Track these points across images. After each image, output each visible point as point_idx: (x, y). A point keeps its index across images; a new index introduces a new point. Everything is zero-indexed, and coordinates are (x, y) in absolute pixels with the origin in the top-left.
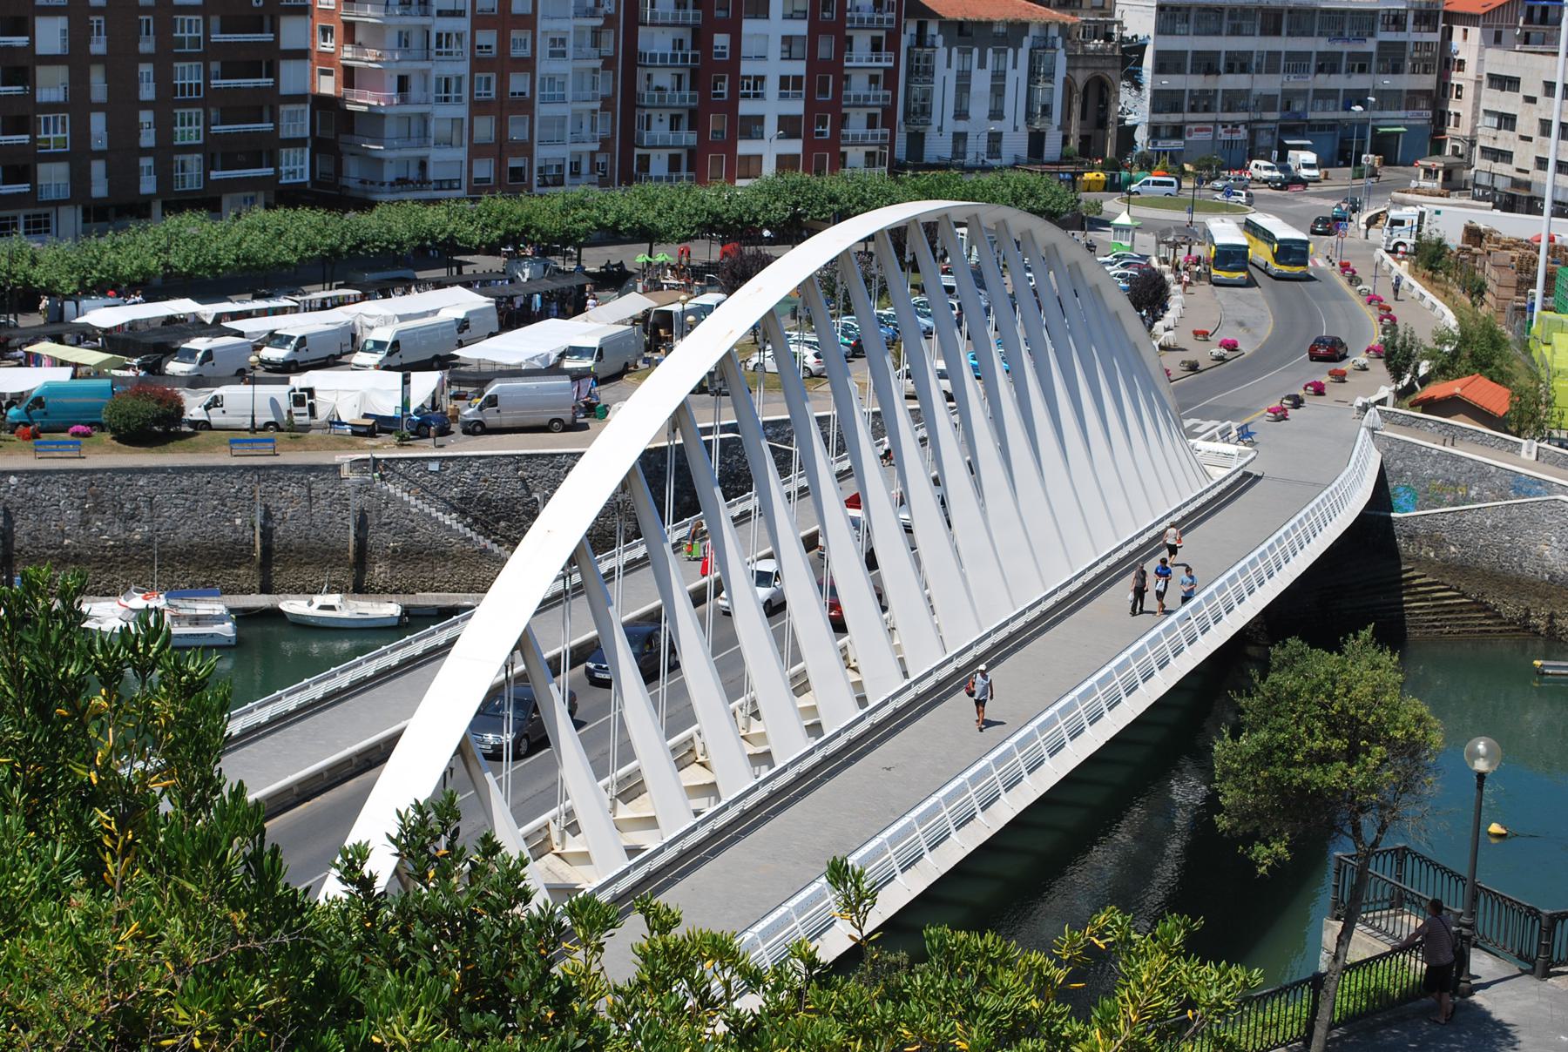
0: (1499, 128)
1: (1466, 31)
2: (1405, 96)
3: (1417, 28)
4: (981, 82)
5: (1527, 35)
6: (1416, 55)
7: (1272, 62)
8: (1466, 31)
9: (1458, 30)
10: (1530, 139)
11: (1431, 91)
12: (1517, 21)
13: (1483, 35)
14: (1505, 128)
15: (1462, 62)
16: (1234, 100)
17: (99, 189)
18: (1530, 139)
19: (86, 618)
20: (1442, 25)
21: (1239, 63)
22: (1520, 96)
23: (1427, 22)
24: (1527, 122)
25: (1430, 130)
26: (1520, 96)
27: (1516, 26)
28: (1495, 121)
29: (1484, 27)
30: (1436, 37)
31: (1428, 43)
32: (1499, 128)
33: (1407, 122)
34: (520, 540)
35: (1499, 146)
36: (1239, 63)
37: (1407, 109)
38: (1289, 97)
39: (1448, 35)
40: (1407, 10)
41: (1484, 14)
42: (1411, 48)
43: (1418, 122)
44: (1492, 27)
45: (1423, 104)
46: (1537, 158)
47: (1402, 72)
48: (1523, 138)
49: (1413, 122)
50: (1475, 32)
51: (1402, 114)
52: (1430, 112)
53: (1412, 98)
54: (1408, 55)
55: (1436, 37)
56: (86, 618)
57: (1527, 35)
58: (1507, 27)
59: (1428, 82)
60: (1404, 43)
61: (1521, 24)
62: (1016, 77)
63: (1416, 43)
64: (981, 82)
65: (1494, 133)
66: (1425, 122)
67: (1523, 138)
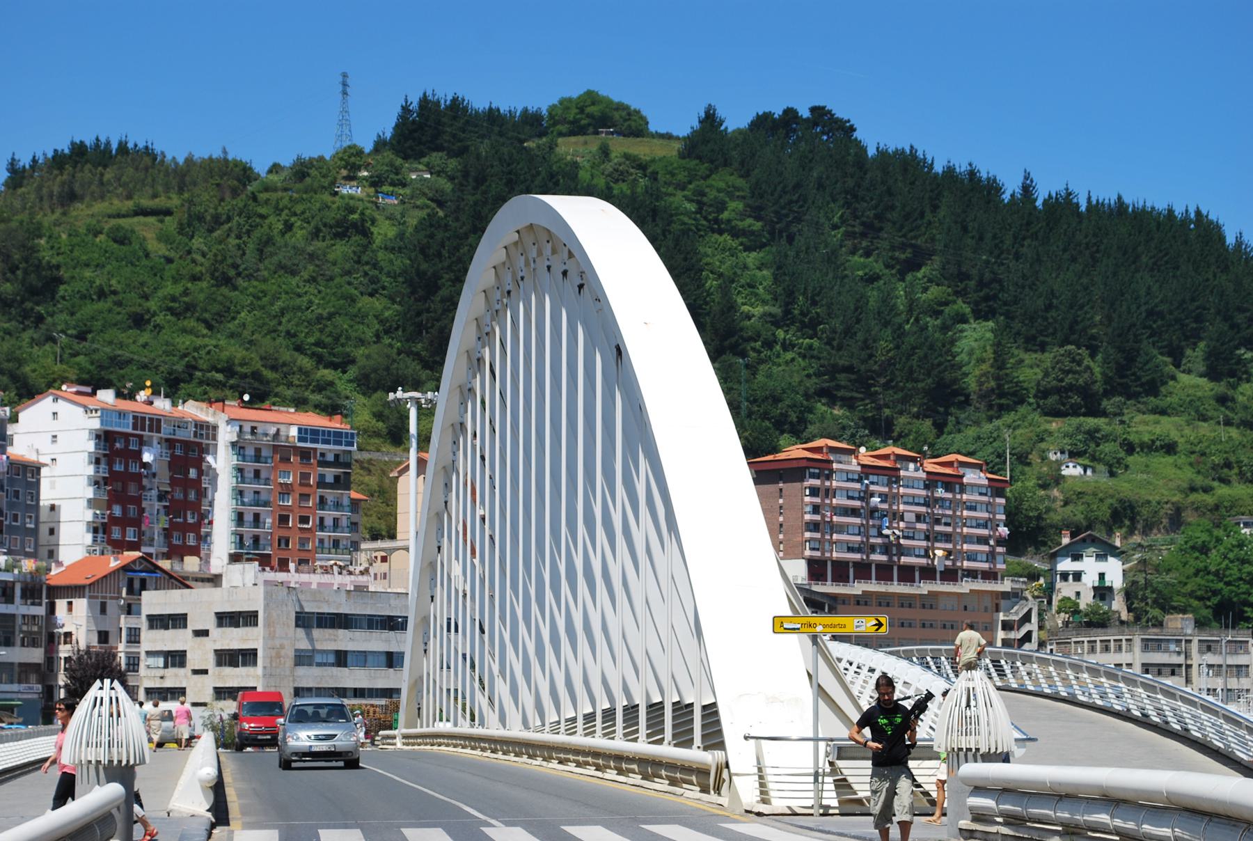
0: (166, 666)
1: (70, 603)
2: (17, 669)
3: (24, 601)
5: (129, 606)
6: (25, 628)
8: (70, 603)
9: (61, 605)
10: (205, 672)
11: (39, 665)
12: (120, 592)
13: (90, 606)
14: (174, 665)
15: (68, 635)
18: (205, 672)
19: (24, 167)
20: (45, 601)
22: (189, 631)
23: (32, 597)
24: (200, 654)
25: (40, 706)
26: (189, 631)
27: (119, 597)
28: (160, 661)
29: (90, 597)
30: (40, 611)
31: (34, 617)
32: (166, 666)
33: (20, 696)
34: (441, 377)
35: (168, 684)
37: (20, 682)
39: (52, 609)
40: (13, 583)
41: (90, 585)
42: (19, 621)
43: (30, 696)
44: (96, 597)
45: (33, 677)
46: (215, 688)
47: (13, 645)
48: (196, 672)
49: (25, 696)
50: (81, 604)
51: (15, 687)
52: (40, 686)
53: (26, 670)
54: (17, 628)
55: (40, 611)
56: (24, 167)
57: (129, 606)
58: (112, 598)
59: (36, 655)
60: (13, 616)
61: (124, 594)
63: (24, 616)
65: (161, 672)
66: (36, 696)
67: (196, 672)
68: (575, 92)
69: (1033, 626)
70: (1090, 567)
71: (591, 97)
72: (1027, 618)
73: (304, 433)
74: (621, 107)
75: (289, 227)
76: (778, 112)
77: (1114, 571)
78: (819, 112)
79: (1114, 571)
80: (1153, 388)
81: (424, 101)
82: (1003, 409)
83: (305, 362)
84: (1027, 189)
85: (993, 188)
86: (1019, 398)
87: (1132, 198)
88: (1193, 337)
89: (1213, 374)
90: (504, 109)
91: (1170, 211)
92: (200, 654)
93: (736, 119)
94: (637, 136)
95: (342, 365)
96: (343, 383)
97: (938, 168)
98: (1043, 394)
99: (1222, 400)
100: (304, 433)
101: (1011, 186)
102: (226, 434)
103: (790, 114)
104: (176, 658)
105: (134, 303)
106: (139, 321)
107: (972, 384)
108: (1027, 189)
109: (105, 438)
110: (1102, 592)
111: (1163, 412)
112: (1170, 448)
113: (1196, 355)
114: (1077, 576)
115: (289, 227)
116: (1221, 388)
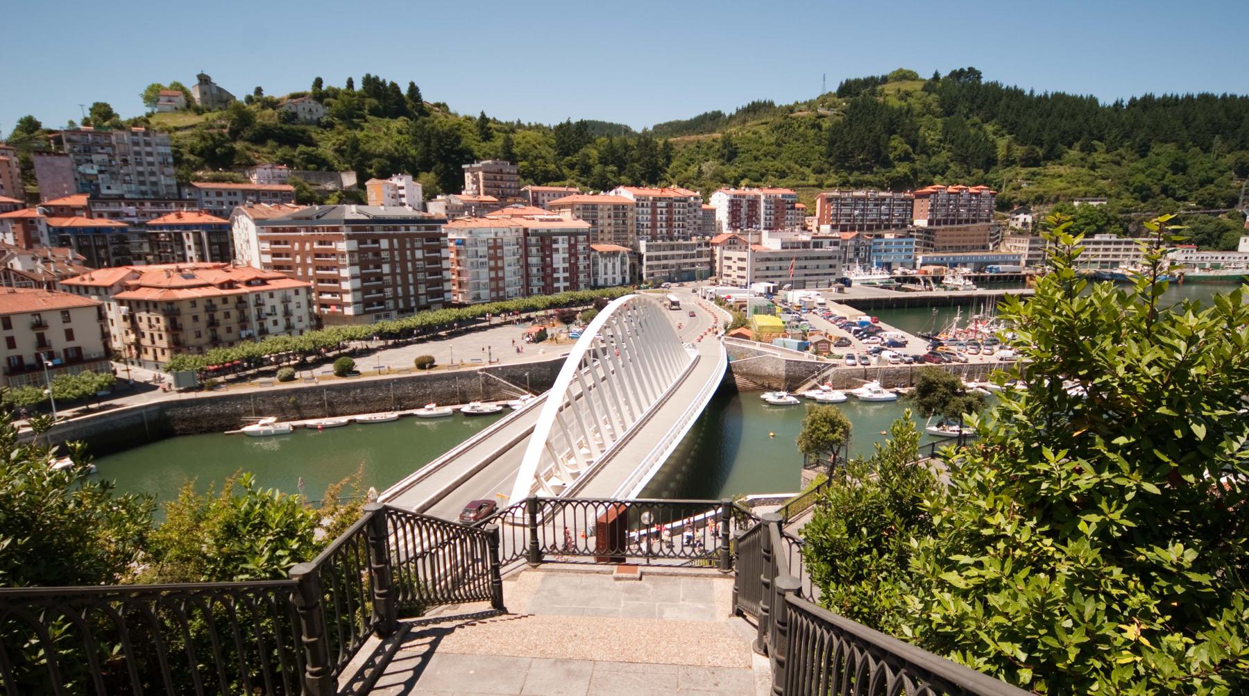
4: (610, 266)
7: (673, 257)
16: (665, 267)
17: (401, 305)
21: (666, 257)
24: (735, 267)
36: (666, 257)
38: (679, 266)
62: (618, 264)
64: (610, 266)
68: (896, 69)
69: (1000, 235)
70: (1022, 217)
71: (901, 70)
72: (998, 232)
73: (783, 196)
74: (910, 72)
75: (800, 126)
76: (958, 69)
77: (1029, 219)
78: (971, 69)
79: (1029, 219)
80: (1059, 157)
81: (847, 81)
82: (1008, 166)
83: (797, 167)
84: (1032, 92)
85: (1021, 93)
86: (1013, 162)
87: (1070, 91)
88: (1078, 139)
89: (1082, 150)
90: (876, 76)
91: (1082, 97)
92: (735, 267)
93: (944, 73)
94: (913, 80)
95: (808, 166)
96: (808, 171)
97: (1004, 87)
98: (1022, 160)
99: (1082, 159)
100: (783, 196)
101: (1027, 93)
102: (763, 198)
103: (962, 70)
104: (730, 267)
105: (755, 153)
106: (756, 158)
107: (1000, 157)
108: (1032, 92)
109: (731, 201)
110: (1025, 224)
111: (1061, 165)
112: (1060, 176)
113: (1077, 145)
114: (1017, 219)
115: (800, 126)
116: (1082, 155)
